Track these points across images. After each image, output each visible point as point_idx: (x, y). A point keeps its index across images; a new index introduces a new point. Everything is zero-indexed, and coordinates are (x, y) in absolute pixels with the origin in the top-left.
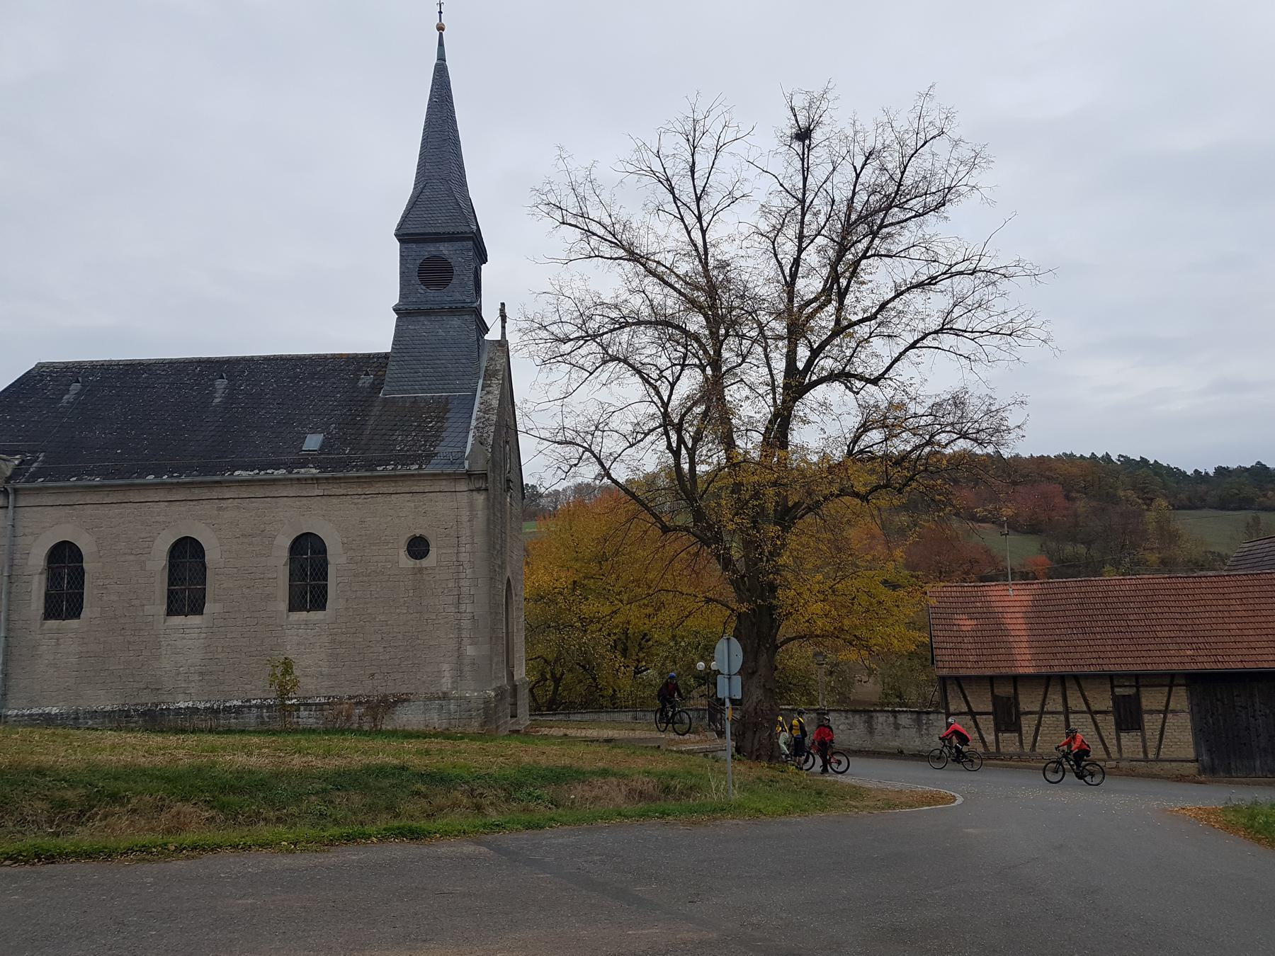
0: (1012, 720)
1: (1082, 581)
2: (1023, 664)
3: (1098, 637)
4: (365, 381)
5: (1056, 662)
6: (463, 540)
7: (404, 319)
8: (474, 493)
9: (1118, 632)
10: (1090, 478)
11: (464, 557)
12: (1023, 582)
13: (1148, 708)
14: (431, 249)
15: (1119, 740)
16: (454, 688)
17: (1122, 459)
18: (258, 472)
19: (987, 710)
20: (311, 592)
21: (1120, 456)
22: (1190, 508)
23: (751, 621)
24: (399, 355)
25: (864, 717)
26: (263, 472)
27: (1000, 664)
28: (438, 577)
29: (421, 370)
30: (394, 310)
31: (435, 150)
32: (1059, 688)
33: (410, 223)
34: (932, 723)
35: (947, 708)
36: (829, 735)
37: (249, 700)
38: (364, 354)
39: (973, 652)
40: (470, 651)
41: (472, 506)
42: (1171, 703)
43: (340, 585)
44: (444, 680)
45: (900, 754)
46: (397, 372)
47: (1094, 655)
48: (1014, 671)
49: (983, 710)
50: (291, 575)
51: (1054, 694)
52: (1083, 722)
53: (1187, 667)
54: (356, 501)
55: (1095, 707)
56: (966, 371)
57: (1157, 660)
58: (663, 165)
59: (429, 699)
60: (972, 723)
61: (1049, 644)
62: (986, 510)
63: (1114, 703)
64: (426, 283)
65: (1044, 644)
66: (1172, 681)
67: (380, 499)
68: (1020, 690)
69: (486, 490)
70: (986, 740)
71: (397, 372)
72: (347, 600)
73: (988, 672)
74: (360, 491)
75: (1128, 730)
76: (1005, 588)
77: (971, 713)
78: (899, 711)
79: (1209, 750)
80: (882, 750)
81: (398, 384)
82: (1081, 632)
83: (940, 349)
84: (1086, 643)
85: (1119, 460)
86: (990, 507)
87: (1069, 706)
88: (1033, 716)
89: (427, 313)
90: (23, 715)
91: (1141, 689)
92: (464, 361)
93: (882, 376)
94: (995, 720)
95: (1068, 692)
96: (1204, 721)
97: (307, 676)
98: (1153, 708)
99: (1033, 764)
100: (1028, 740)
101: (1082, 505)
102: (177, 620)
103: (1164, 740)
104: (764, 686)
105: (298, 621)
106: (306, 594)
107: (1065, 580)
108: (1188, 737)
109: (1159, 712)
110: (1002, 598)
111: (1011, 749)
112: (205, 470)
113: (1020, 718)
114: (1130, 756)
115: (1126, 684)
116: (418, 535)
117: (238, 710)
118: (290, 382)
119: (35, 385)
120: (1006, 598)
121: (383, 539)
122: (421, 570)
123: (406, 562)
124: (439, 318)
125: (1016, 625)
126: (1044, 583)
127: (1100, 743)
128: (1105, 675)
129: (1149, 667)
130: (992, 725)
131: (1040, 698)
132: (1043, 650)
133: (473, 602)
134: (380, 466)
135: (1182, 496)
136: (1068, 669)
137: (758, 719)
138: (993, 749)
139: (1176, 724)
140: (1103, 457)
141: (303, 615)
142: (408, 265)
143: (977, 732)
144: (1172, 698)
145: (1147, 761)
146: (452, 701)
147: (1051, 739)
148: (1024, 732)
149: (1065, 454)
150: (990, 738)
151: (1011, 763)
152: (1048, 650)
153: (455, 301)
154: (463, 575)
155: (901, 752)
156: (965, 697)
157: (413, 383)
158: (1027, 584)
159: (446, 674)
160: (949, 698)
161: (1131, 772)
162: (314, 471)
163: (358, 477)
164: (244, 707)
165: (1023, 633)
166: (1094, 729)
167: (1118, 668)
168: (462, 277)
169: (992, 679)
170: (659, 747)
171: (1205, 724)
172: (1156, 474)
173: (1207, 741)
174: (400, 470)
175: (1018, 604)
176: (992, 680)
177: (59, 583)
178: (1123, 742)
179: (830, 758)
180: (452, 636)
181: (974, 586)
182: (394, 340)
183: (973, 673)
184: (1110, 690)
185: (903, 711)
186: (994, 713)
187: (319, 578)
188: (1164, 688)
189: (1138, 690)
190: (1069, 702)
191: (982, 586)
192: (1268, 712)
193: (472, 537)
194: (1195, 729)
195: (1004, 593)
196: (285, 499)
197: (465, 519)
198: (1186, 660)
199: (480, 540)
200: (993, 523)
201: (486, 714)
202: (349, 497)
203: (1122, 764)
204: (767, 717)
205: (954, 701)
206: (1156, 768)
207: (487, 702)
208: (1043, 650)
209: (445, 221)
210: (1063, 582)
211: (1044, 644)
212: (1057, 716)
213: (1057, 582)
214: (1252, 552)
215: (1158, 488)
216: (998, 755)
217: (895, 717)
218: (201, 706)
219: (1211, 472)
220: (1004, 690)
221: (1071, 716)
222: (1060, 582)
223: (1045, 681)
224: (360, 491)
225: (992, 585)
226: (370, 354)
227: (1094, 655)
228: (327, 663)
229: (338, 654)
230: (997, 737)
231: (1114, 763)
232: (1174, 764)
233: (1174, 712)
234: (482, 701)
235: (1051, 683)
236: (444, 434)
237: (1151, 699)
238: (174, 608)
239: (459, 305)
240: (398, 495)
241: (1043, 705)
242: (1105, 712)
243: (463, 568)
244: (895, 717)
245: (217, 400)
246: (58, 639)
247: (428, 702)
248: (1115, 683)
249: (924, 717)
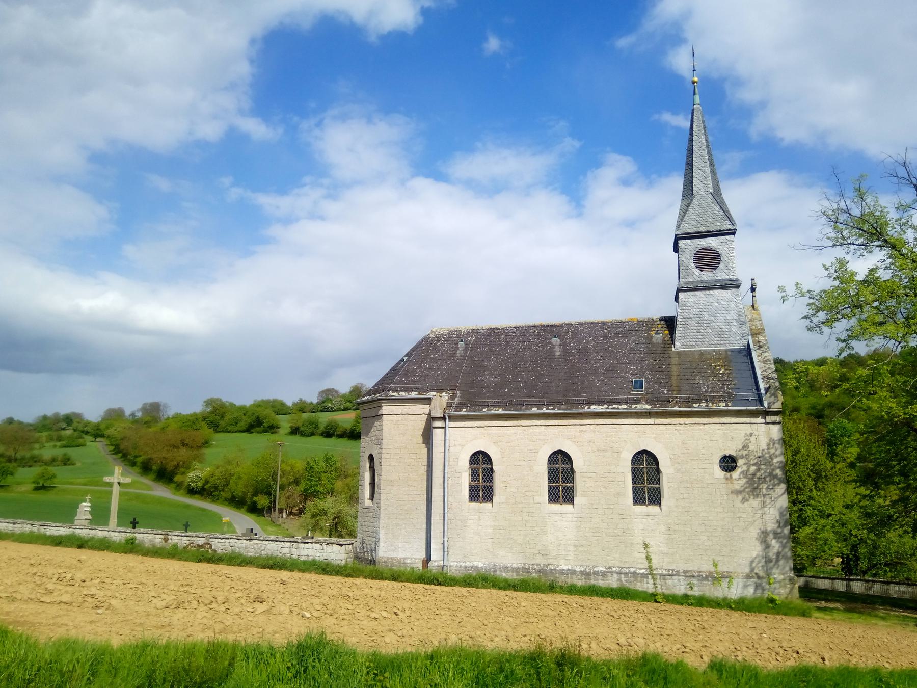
18: (607, 406)
20: (648, 493)
26: (610, 407)
37: (610, 568)
90: (461, 566)
102: (556, 507)
112: (569, 404)
117: (604, 575)
119: (436, 344)
123: (720, 474)
164: (608, 572)
177: (477, 478)
218: (578, 569)
238: (638, 499)
245: (558, 354)
246: (479, 516)
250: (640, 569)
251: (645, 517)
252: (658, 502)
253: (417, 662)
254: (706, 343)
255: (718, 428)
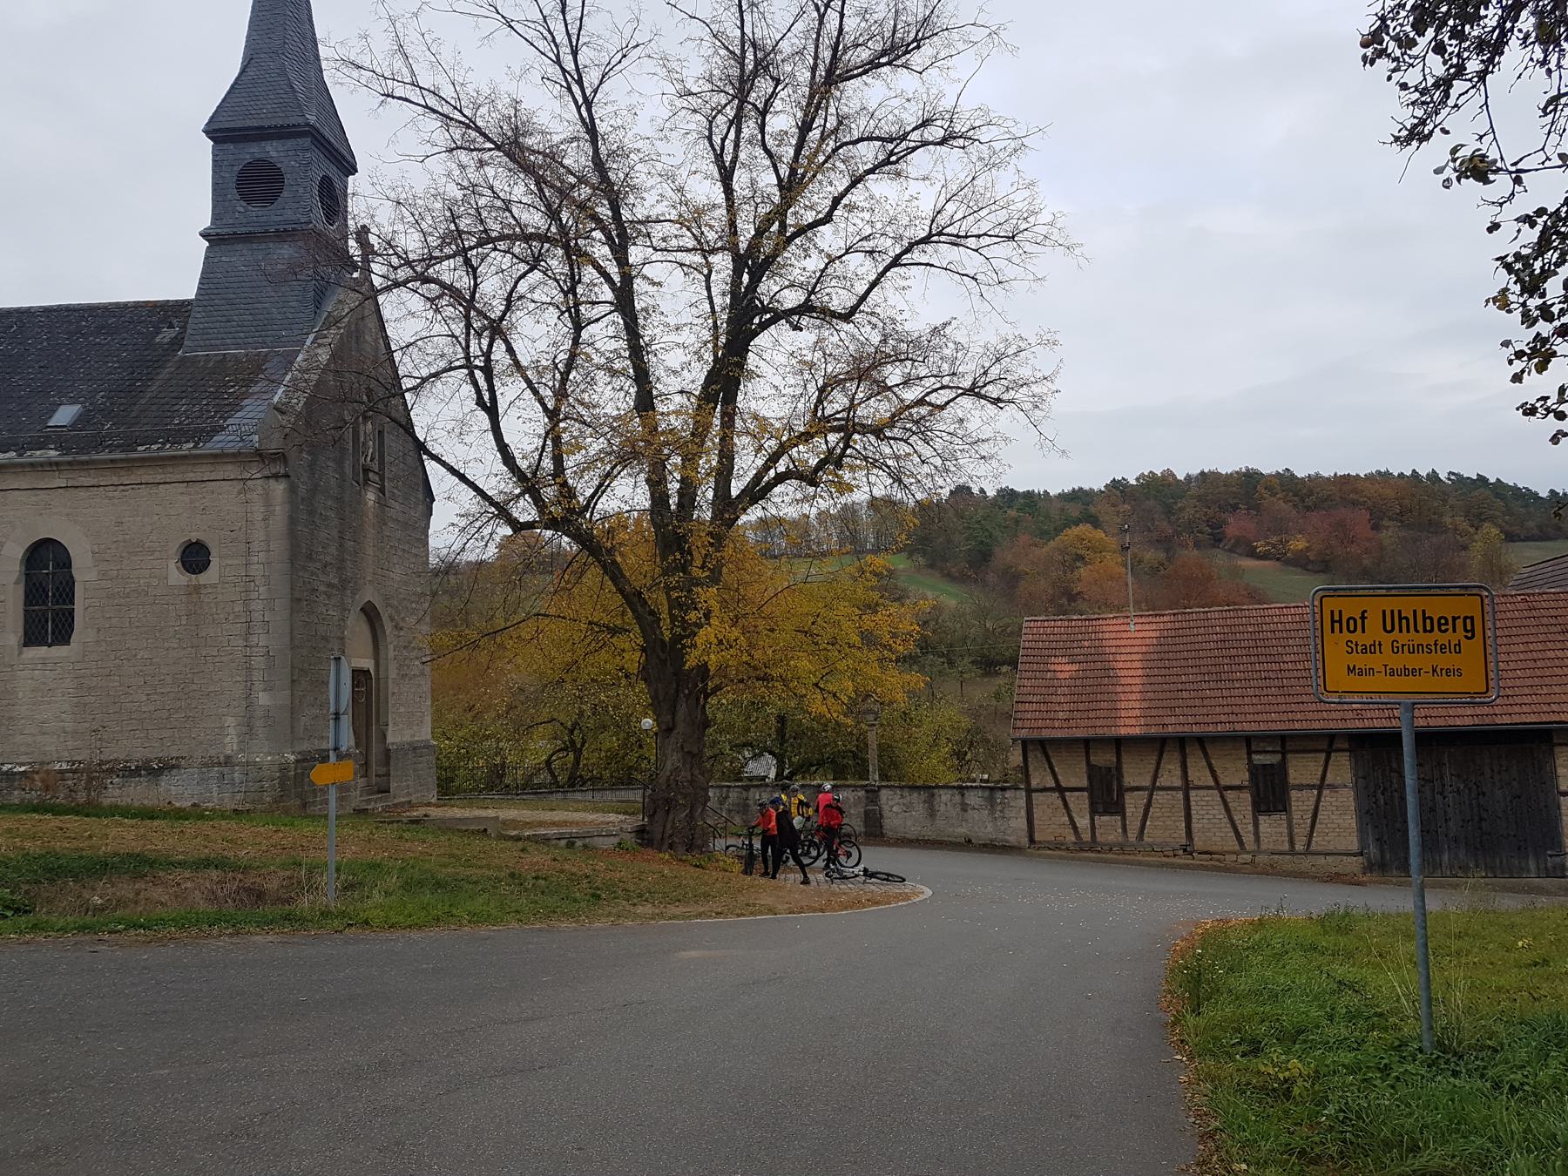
0: (1113, 799)
1: (1229, 611)
2: (1128, 722)
4: (167, 335)
5: (1173, 720)
6: (255, 546)
7: (217, 249)
8: (271, 480)
9: (1265, 679)
12: (1151, 613)
13: (1297, 782)
14: (253, 151)
15: (1256, 825)
16: (242, 750)
17: (1453, 477)
19: (1079, 785)
20: (53, 621)
21: (1450, 473)
22: (1540, 539)
23: (658, 656)
24: (207, 297)
25: (924, 795)
27: (1098, 723)
28: (220, 597)
30: (201, 234)
31: (265, 13)
32: (1177, 755)
33: (225, 114)
34: (1009, 803)
35: (1028, 783)
36: (837, 818)
38: (177, 301)
39: (1066, 707)
40: (263, 699)
41: (267, 499)
43: (90, 609)
45: (967, 845)
46: (203, 320)
47: (1226, 710)
48: (1114, 732)
49: (1074, 785)
50: (27, 596)
53: (1350, 724)
54: (110, 494)
55: (1224, 782)
56: (975, 298)
57: (1310, 716)
59: (205, 765)
60: (1060, 802)
62: (1268, 544)
63: (1251, 774)
64: (247, 197)
65: (1161, 696)
67: (144, 490)
68: (1125, 758)
69: (287, 476)
70: (1078, 825)
71: (203, 320)
72: (99, 630)
73: (1079, 733)
74: (115, 480)
75: (1268, 812)
77: (1060, 789)
78: (967, 787)
79: (1378, 840)
80: (946, 839)
81: (205, 337)
83: (932, 265)
85: (1449, 479)
86: (1274, 540)
89: (247, 238)
91: (1289, 756)
92: (294, 304)
93: (854, 310)
94: (1091, 797)
96: (1374, 800)
97: (45, 733)
99: (1140, 858)
100: (1134, 825)
101: (1390, 534)
103: (1317, 826)
105: (33, 658)
106: (47, 622)
107: (1207, 609)
108: (1351, 821)
109: (1312, 787)
110: (1119, 635)
111: (1111, 838)
118: (67, 339)
120: (1124, 635)
121: (147, 545)
123: (177, 577)
124: (263, 246)
125: (1131, 671)
126: (1177, 614)
129: (1297, 725)
130: (1086, 804)
131: (1152, 767)
132: (1160, 704)
133: (268, 632)
134: (143, 445)
135: (1531, 524)
138: (1087, 837)
139: (1334, 804)
140: (1428, 474)
141: (42, 651)
144: (1330, 768)
146: (237, 768)
147: (1165, 826)
149: (1379, 472)
150: (1083, 822)
151: (1110, 856)
152: (1165, 704)
153: (286, 222)
154: (254, 595)
157: (224, 336)
159: (231, 730)
162: (53, 453)
163: (112, 461)
165: (1138, 681)
166: (1223, 811)
167: (1254, 727)
168: (295, 188)
169: (1087, 743)
170: (485, 830)
172: (1497, 495)
173: (1377, 827)
174: (169, 451)
175: (1139, 642)
178: (1262, 828)
179: (837, 849)
180: (238, 679)
182: (202, 278)
186: (1090, 789)
187: (37, 602)
188: (1318, 755)
189: (1284, 758)
190: (1189, 774)
191: (1095, 620)
193: (268, 542)
196: (16, 492)
197: (258, 517)
198: (1350, 715)
199: (279, 547)
200: (1278, 559)
201: (282, 785)
202: (101, 489)
203: (1261, 858)
205: (1037, 774)
206: (1306, 863)
207: (283, 769)
208: (1160, 704)
209: (271, 110)
210: (1203, 612)
211: (1161, 696)
212: (1174, 793)
215: (1499, 514)
216: (1093, 846)
217: (963, 795)
220: (1104, 758)
221: (1193, 793)
223: (1158, 745)
224: (115, 480)
225: (1110, 618)
226: (184, 301)
227: (1226, 710)
228: (73, 716)
229: (86, 705)
231: (1248, 857)
233: (1332, 787)
234: (276, 768)
235: (1167, 748)
236: (246, 402)
237: (1302, 770)
238: (33, 637)
240: (167, 485)
241: (1155, 777)
242: (1239, 788)
243: (255, 586)
244: (963, 795)
245: (686, 668)
248: (1253, 748)
249: (999, 794)
250: (22, 764)
251: (39, 666)
252: (63, 638)
253: (1501, 862)
254: (239, 341)
255: (180, 491)
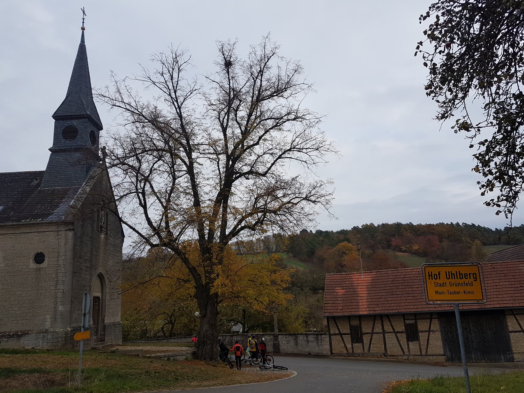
0: (359, 337)
1: (395, 270)
2: (363, 310)
3: (399, 296)
4: (35, 182)
5: (378, 309)
6: (61, 254)
7: (54, 154)
9: (408, 294)
10: (450, 233)
11: (61, 262)
13: (421, 330)
14: (69, 123)
16: (52, 327)
17: (464, 225)
21: (463, 223)
22: (495, 245)
24: (50, 170)
25: (294, 337)
29: (59, 177)
30: (49, 150)
40: (60, 308)
42: (431, 327)
44: (47, 323)
45: (309, 355)
46: (48, 178)
47: (396, 305)
51: (378, 324)
52: (391, 337)
53: (437, 309)
54: (11, 237)
55: (397, 330)
58: (165, 79)
60: (341, 339)
61: (376, 300)
62: (406, 247)
64: (65, 138)
66: (431, 316)
67: (23, 235)
68: (362, 323)
69: (73, 230)
72: (3, 285)
74: (13, 232)
75: (412, 340)
76: (360, 274)
77: (341, 334)
79: (450, 350)
82: (391, 294)
83: (292, 158)
84: (392, 299)
85: (463, 225)
86: (408, 246)
87: (385, 329)
88: (368, 335)
89: (64, 151)
91: (418, 320)
93: (266, 173)
94: (351, 337)
95: (384, 323)
98: (424, 330)
99: (369, 358)
104: (209, 322)
107: (387, 270)
108: (440, 343)
109: (426, 331)
111: (359, 351)
113: (362, 336)
114: (414, 353)
115: (410, 318)
116: (39, 252)
120: (360, 279)
121: (23, 254)
122: (39, 269)
123: (33, 265)
124: (70, 153)
125: (363, 292)
127: (400, 347)
128: (401, 314)
129: (420, 310)
131: (372, 326)
135: (490, 239)
136: (383, 312)
137: (204, 339)
138: (350, 351)
142: (58, 130)
143: (343, 343)
145: (422, 356)
146: (49, 334)
148: (364, 343)
149: (440, 223)
150: (349, 346)
154: (60, 271)
155: (310, 354)
156: (337, 326)
158: (370, 272)
159: (48, 320)
160: (330, 327)
161: (414, 361)
163: (12, 225)
165: (365, 295)
167: (405, 310)
168: (82, 134)
170: (138, 355)
171: (448, 337)
172: (479, 230)
174: (33, 221)
175: (365, 282)
176: (349, 318)
178: (411, 346)
180: (52, 301)
181: (347, 274)
183: (340, 314)
184: (403, 321)
185: (310, 334)
186: (351, 334)
188: (428, 320)
192: (476, 330)
194: (443, 339)
195: (359, 277)
200: (409, 252)
202: (8, 235)
203: (410, 357)
204: (209, 338)
206: (426, 359)
212: (380, 335)
213: (383, 271)
214: (493, 258)
216: (353, 354)
217: (307, 337)
219: (503, 229)
220: (355, 323)
221: (386, 335)
222: (385, 271)
223: (373, 318)
224: (13, 232)
227: (396, 305)
230: (352, 345)
231: (406, 357)
232: (434, 357)
233: (433, 331)
236: (61, 205)
237: (422, 325)
239: (79, 147)
241: (373, 329)
244: (307, 337)
247: (37, 335)
248: (406, 318)
249: (319, 336)
